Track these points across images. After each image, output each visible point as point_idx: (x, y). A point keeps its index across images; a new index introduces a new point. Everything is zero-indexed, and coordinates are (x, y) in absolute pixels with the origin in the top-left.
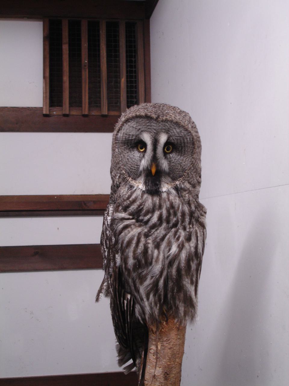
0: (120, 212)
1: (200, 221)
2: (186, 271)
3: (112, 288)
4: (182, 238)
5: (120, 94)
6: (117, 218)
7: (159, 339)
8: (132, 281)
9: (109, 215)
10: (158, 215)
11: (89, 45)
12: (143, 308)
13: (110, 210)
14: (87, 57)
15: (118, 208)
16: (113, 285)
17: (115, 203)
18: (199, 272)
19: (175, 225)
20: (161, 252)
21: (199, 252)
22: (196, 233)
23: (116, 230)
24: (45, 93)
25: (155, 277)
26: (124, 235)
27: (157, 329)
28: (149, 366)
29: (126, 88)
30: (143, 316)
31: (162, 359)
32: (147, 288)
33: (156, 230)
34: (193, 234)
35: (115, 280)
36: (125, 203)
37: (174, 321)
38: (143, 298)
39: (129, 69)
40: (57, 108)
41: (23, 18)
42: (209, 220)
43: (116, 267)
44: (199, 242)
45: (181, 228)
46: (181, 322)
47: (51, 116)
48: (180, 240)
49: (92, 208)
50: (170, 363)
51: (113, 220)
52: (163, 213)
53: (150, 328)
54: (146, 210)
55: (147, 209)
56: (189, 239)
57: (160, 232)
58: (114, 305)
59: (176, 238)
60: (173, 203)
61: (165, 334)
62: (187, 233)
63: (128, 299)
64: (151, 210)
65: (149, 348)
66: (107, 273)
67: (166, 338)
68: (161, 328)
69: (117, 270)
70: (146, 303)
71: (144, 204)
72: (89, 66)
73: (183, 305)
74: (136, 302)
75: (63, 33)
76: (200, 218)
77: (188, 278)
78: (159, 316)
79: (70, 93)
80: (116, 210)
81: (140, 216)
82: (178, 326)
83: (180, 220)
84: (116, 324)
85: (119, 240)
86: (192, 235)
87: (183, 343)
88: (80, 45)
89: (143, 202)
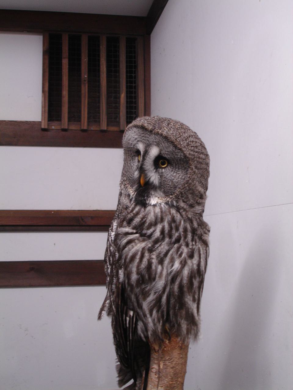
0: (125, 227)
1: (203, 239)
2: (188, 289)
3: (114, 305)
4: (185, 255)
5: (119, 109)
6: (121, 233)
7: (162, 358)
8: (135, 297)
9: (113, 230)
10: (160, 229)
11: (89, 60)
12: (145, 325)
13: (114, 225)
14: (87, 72)
15: (122, 224)
16: (116, 302)
17: (119, 218)
18: (201, 290)
19: (178, 240)
20: (165, 268)
21: (201, 270)
22: (199, 250)
23: (120, 246)
24: (43, 107)
25: (157, 293)
26: (127, 250)
27: (159, 347)
28: (150, 386)
29: (125, 103)
30: (145, 333)
31: (164, 379)
32: (150, 305)
33: (160, 245)
34: (196, 252)
35: (117, 296)
36: (129, 216)
37: (176, 340)
38: (147, 314)
39: (129, 84)
40: (56, 122)
41: (23, 32)
42: (212, 238)
43: (119, 283)
44: (202, 260)
45: (183, 244)
46: (184, 341)
47: (49, 130)
48: (183, 256)
49: (91, 224)
50: (172, 383)
51: (117, 235)
52: (165, 227)
53: (152, 347)
54: (149, 224)
55: (149, 222)
56: (191, 256)
57: (164, 247)
58: (116, 322)
59: (178, 254)
60: (174, 217)
61: (168, 353)
62: (190, 250)
63: (130, 315)
64: (153, 223)
65: (151, 367)
66: (110, 290)
67: (169, 357)
68: (163, 347)
69: (120, 286)
70: (150, 320)
71: (146, 216)
72: (88, 81)
73: (186, 322)
74: (139, 320)
75: (63, 47)
76: (204, 236)
77: (190, 295)
78: (162, 333)
79: (69, 108)
80: (120, 225)
81: (143, 229)
82: (181, 345)
83: (182, 235)
84: (118, 343)
85: (123, 255)
86: (195, 252)
87: (186, 362)
88: (80, 60)
89: (146, 215)
